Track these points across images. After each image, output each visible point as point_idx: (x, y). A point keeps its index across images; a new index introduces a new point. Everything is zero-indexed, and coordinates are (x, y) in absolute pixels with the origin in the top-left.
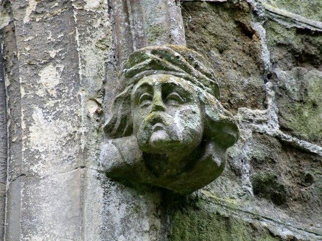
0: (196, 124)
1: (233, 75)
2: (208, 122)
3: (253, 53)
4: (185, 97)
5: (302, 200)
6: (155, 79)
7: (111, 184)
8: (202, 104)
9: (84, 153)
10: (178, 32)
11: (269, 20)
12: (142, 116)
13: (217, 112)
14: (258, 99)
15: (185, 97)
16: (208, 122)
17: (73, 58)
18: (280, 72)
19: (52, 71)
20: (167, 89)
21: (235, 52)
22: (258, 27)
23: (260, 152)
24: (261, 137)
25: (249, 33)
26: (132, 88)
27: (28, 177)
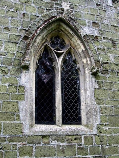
0: (96, 71)
1: (99, 66)
2: (97, 70)
3: (100, 64)
4: (95, 69)
5: (104, 73)
6: (93, 68)
7: (68, 14)
8: (96, 69)
9: (89, 73)
10: (94, 64)
11: (101, 62)
12: (93, 70)
13: (97, 70)
14: (101, 67)
15: (95, 69)
16: (97, 70)
17: (88, 67)
18: (102, 65)
19: (109, 51)
20: (94, 69)
21: (99, 65)
22: (100, 62)
23: (101, 71)
24: (101, 70)
25: (100, 63)
26: (32, 41)
27: (86, 75)
